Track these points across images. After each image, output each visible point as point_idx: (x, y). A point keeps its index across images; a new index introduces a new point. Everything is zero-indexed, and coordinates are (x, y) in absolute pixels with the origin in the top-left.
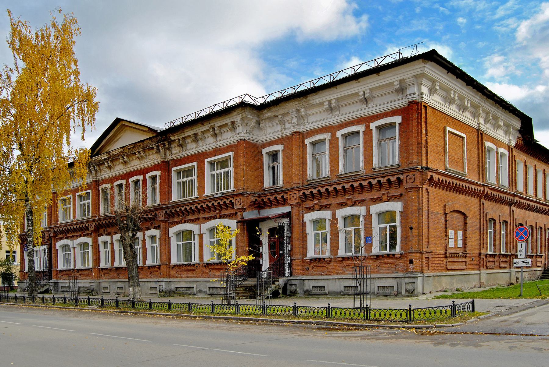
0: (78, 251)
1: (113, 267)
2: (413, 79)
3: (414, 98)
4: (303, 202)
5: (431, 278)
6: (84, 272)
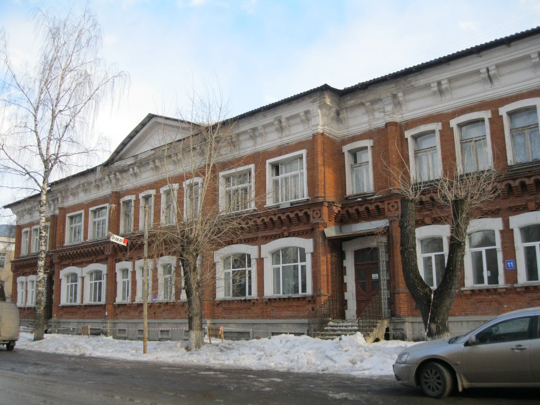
0: (88, 282)
1: (134, 303)
6: (93, 309)
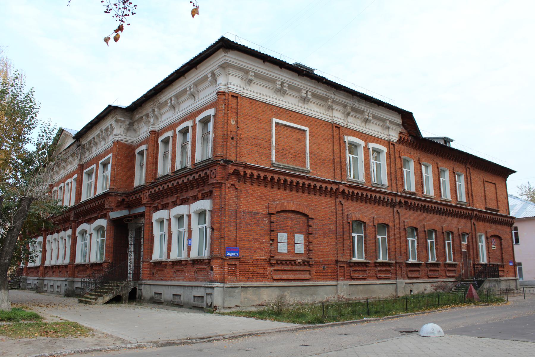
2: (219, 69)
3: (220, 89)
5: (237, 290)
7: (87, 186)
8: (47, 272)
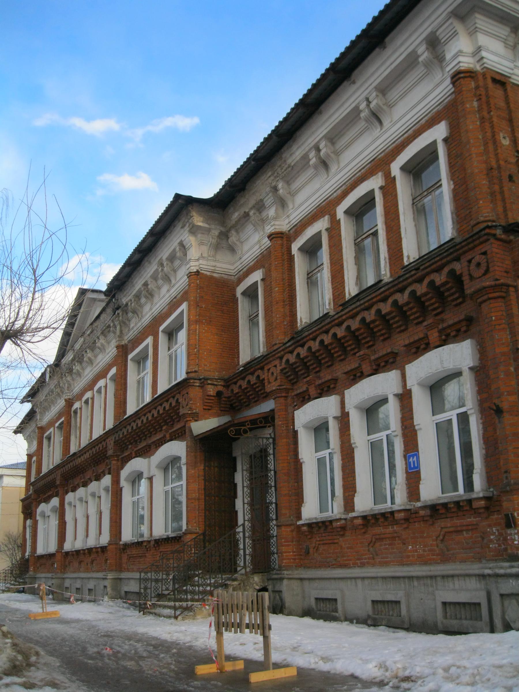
4: (293, 384)
7: (136, 385)
8: (70, 563)
